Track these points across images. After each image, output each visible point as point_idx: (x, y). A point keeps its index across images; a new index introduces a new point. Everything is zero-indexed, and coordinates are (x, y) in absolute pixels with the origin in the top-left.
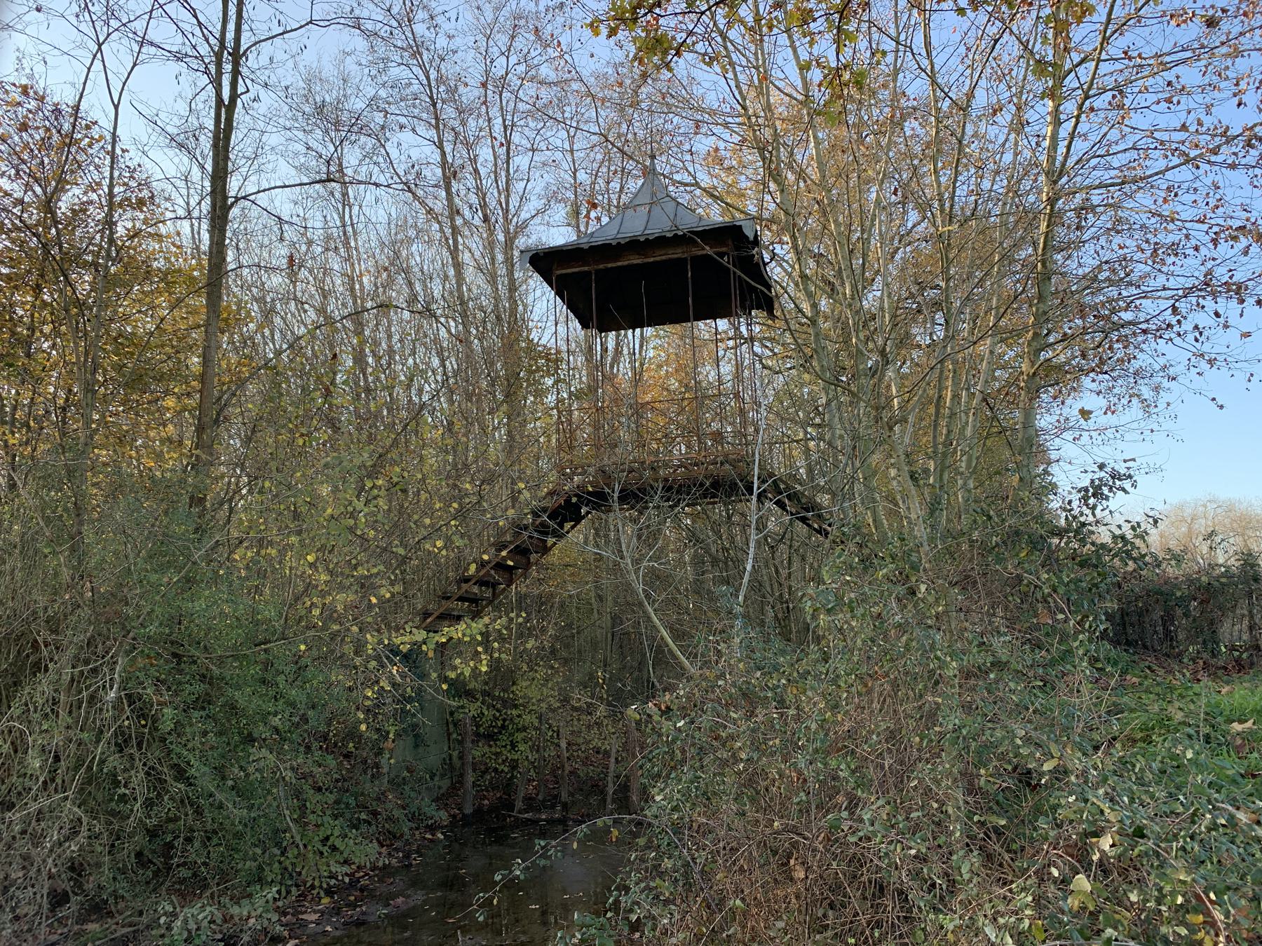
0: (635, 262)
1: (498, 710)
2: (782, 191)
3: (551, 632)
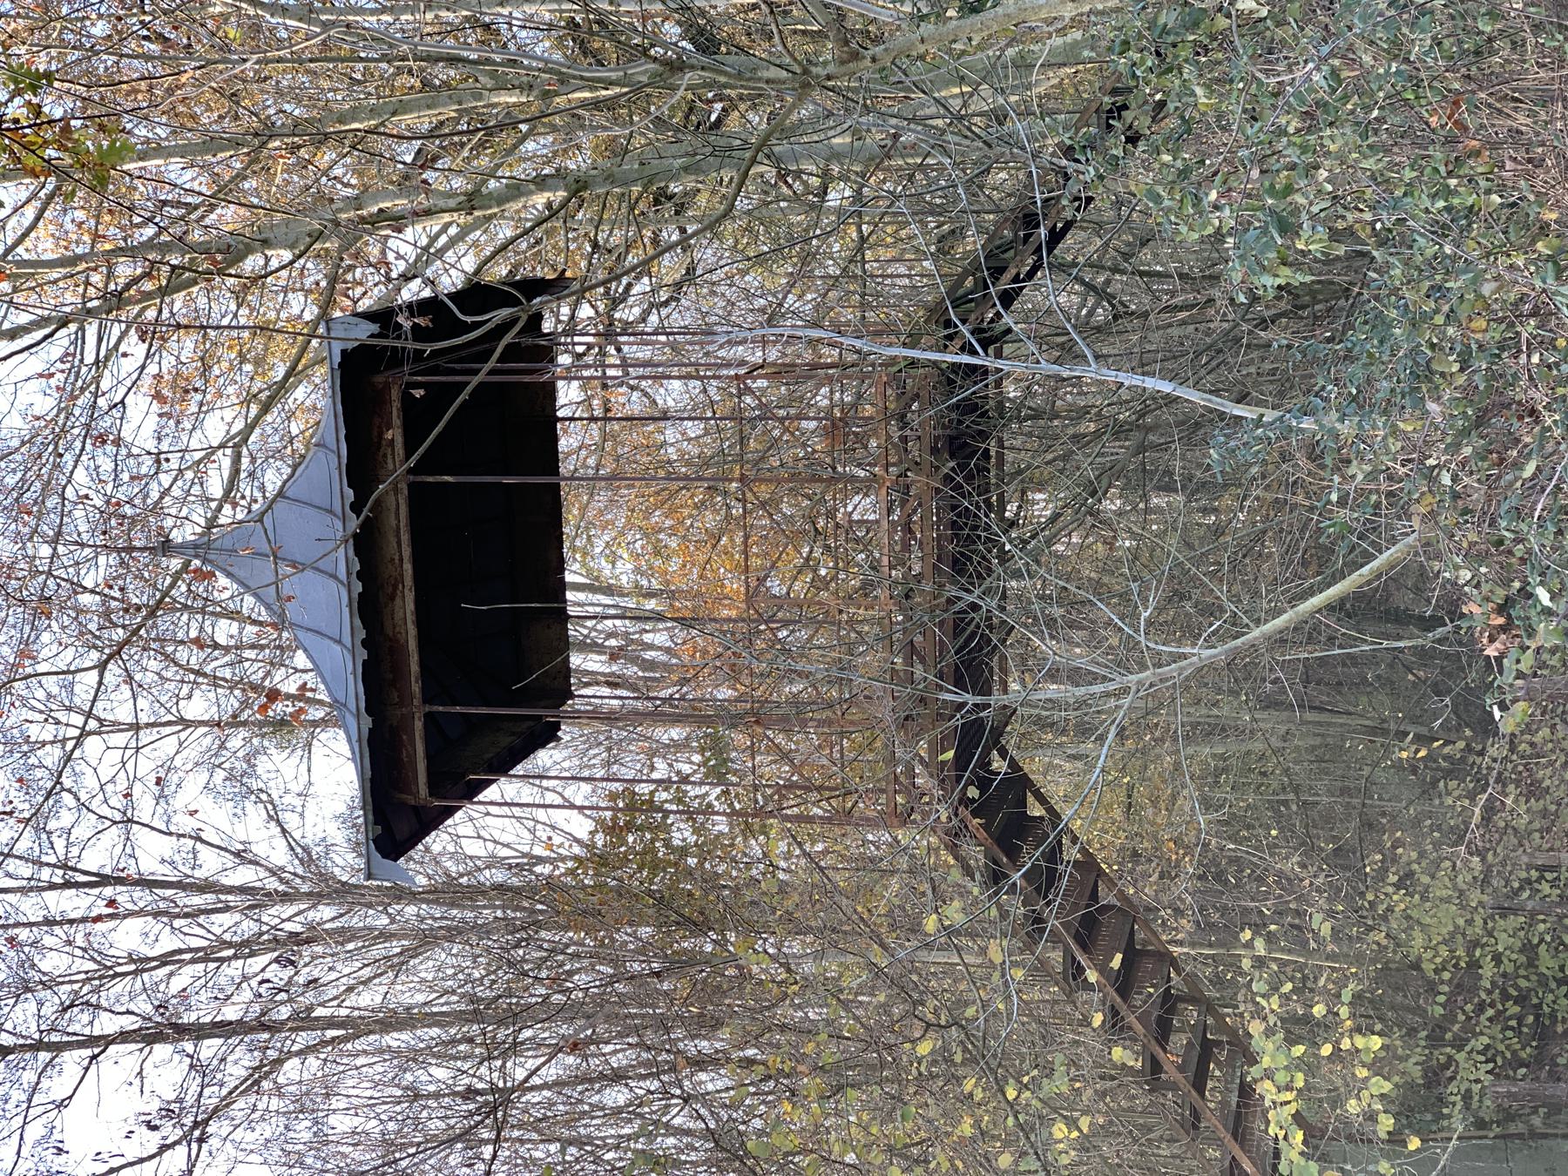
1: (1481, 1008)
2: (266, 243)
3: (1292, 864)
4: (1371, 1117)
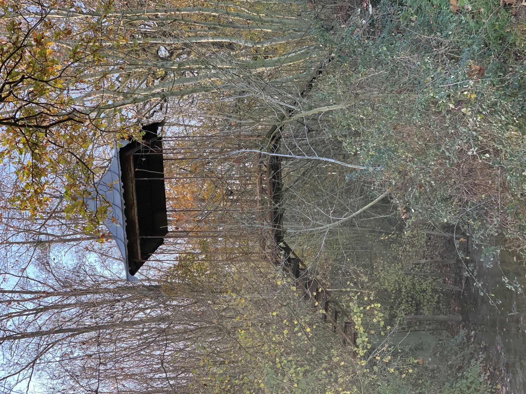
0: (136, 211)
4: (379, 322)
